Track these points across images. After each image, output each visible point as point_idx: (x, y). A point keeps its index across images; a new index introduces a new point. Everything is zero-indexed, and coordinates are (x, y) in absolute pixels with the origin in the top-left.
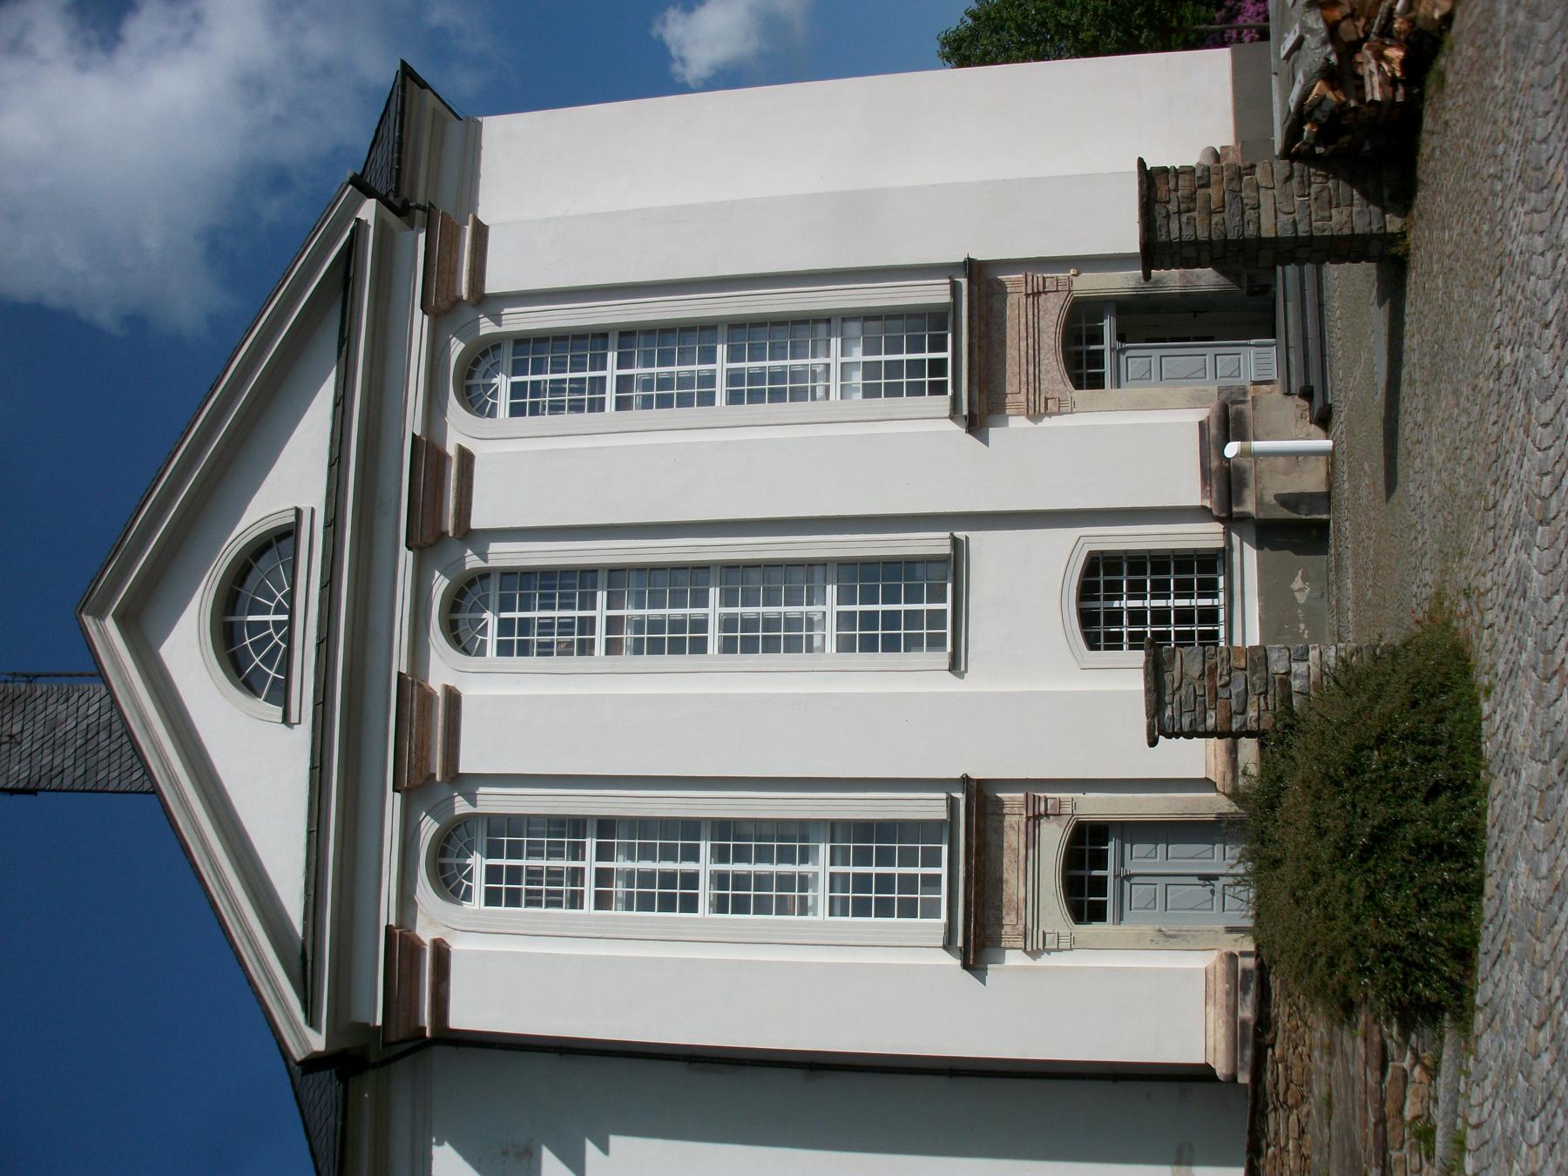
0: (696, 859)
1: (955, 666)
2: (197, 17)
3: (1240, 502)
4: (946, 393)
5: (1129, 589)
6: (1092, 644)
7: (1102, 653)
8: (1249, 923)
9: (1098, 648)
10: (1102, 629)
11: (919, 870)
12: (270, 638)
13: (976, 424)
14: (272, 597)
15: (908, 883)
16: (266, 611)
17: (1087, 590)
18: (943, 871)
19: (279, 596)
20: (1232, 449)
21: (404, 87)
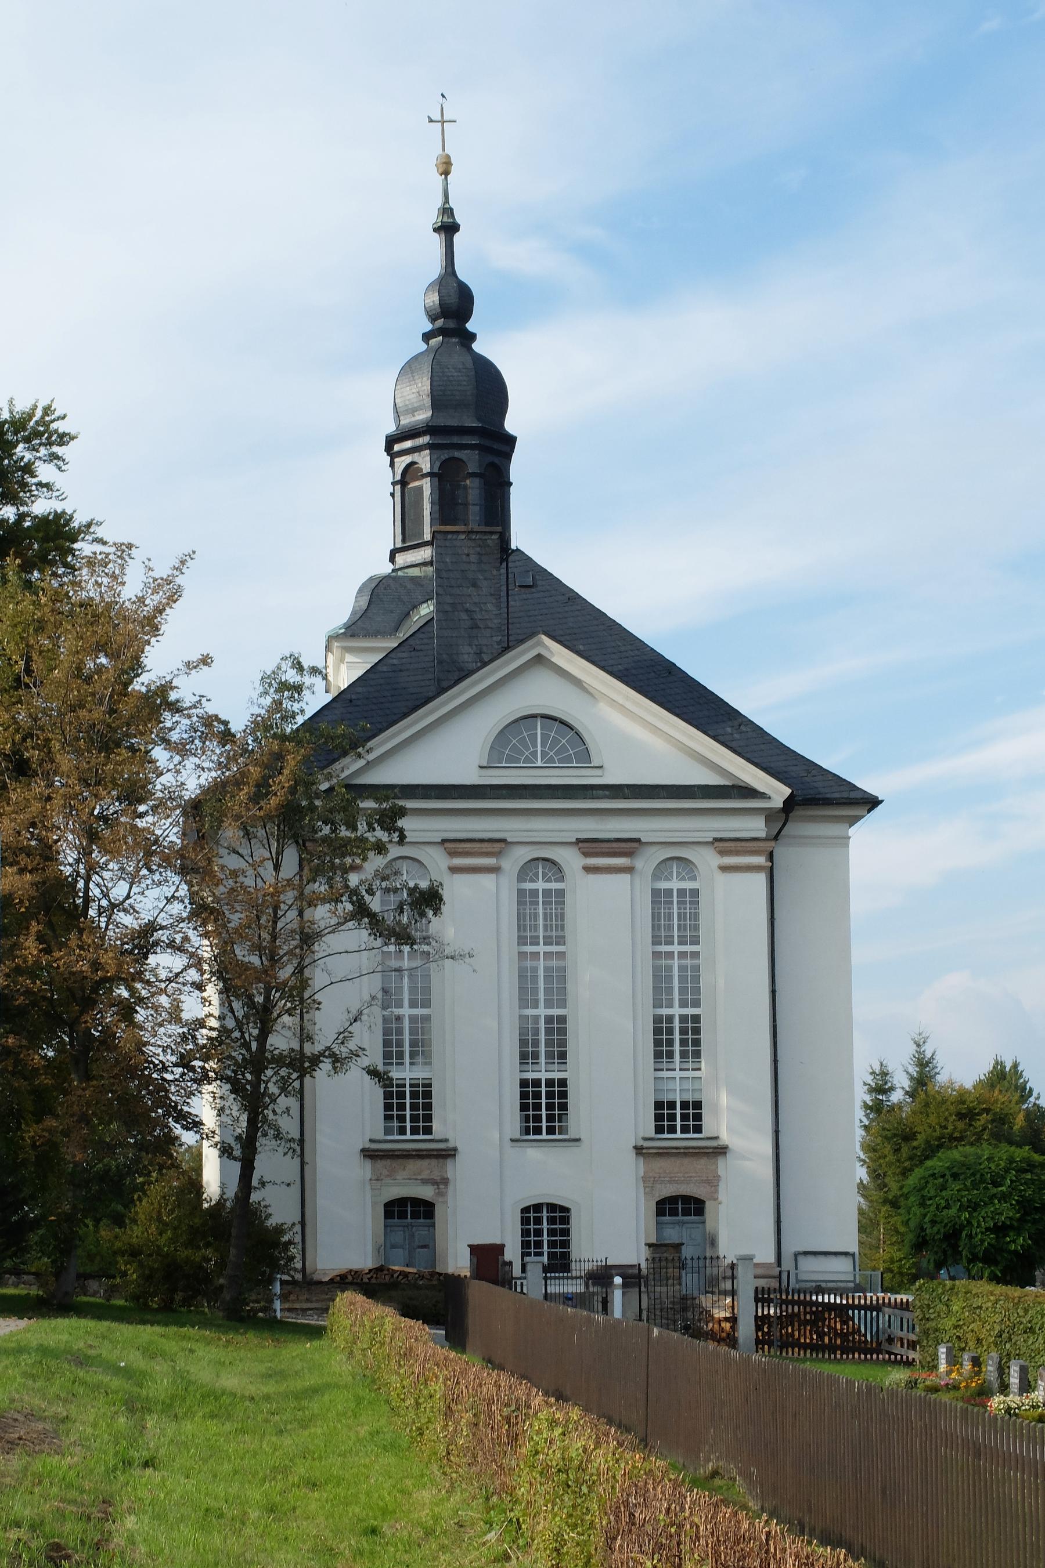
0: (411, 1006)
1: (512, 1140)
2: (19, 424)
3: (594, 1285)
4: (385, 1134)
5: (552, 1229)
6: (525, 1210)
7: (519, 1215)
8: (854, 1248)
9: (522, 1213)
10: (532, 1215)
11: (408, 1124)
12: (556, 754)
13: (368, 1154)
14: (550, 749)
15: (402, 1119)
16: (543, 745)
17: (552, 1207)
18: (408, 1136)
19: (551, 753)
20: (618, 1280)
21: (870, 802)
